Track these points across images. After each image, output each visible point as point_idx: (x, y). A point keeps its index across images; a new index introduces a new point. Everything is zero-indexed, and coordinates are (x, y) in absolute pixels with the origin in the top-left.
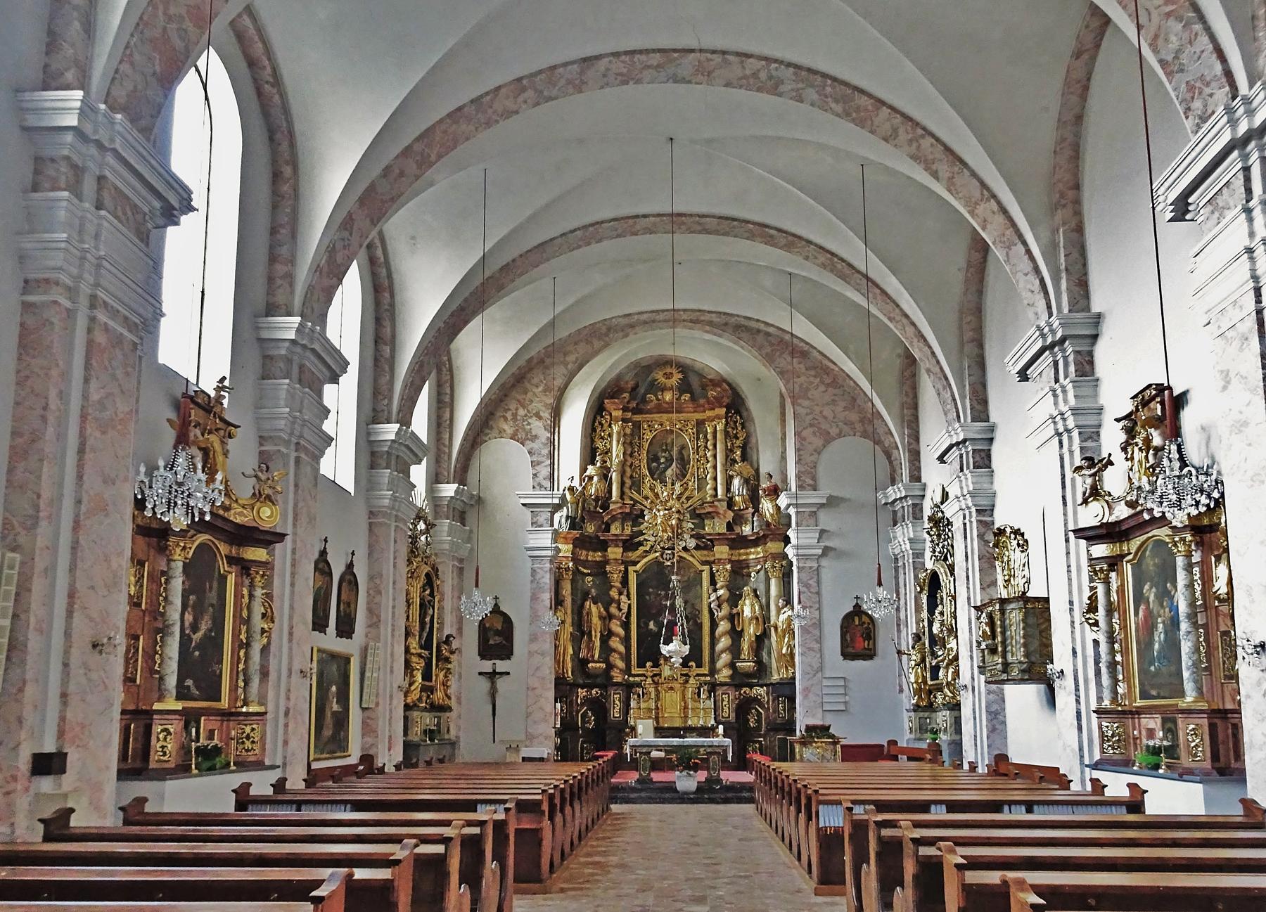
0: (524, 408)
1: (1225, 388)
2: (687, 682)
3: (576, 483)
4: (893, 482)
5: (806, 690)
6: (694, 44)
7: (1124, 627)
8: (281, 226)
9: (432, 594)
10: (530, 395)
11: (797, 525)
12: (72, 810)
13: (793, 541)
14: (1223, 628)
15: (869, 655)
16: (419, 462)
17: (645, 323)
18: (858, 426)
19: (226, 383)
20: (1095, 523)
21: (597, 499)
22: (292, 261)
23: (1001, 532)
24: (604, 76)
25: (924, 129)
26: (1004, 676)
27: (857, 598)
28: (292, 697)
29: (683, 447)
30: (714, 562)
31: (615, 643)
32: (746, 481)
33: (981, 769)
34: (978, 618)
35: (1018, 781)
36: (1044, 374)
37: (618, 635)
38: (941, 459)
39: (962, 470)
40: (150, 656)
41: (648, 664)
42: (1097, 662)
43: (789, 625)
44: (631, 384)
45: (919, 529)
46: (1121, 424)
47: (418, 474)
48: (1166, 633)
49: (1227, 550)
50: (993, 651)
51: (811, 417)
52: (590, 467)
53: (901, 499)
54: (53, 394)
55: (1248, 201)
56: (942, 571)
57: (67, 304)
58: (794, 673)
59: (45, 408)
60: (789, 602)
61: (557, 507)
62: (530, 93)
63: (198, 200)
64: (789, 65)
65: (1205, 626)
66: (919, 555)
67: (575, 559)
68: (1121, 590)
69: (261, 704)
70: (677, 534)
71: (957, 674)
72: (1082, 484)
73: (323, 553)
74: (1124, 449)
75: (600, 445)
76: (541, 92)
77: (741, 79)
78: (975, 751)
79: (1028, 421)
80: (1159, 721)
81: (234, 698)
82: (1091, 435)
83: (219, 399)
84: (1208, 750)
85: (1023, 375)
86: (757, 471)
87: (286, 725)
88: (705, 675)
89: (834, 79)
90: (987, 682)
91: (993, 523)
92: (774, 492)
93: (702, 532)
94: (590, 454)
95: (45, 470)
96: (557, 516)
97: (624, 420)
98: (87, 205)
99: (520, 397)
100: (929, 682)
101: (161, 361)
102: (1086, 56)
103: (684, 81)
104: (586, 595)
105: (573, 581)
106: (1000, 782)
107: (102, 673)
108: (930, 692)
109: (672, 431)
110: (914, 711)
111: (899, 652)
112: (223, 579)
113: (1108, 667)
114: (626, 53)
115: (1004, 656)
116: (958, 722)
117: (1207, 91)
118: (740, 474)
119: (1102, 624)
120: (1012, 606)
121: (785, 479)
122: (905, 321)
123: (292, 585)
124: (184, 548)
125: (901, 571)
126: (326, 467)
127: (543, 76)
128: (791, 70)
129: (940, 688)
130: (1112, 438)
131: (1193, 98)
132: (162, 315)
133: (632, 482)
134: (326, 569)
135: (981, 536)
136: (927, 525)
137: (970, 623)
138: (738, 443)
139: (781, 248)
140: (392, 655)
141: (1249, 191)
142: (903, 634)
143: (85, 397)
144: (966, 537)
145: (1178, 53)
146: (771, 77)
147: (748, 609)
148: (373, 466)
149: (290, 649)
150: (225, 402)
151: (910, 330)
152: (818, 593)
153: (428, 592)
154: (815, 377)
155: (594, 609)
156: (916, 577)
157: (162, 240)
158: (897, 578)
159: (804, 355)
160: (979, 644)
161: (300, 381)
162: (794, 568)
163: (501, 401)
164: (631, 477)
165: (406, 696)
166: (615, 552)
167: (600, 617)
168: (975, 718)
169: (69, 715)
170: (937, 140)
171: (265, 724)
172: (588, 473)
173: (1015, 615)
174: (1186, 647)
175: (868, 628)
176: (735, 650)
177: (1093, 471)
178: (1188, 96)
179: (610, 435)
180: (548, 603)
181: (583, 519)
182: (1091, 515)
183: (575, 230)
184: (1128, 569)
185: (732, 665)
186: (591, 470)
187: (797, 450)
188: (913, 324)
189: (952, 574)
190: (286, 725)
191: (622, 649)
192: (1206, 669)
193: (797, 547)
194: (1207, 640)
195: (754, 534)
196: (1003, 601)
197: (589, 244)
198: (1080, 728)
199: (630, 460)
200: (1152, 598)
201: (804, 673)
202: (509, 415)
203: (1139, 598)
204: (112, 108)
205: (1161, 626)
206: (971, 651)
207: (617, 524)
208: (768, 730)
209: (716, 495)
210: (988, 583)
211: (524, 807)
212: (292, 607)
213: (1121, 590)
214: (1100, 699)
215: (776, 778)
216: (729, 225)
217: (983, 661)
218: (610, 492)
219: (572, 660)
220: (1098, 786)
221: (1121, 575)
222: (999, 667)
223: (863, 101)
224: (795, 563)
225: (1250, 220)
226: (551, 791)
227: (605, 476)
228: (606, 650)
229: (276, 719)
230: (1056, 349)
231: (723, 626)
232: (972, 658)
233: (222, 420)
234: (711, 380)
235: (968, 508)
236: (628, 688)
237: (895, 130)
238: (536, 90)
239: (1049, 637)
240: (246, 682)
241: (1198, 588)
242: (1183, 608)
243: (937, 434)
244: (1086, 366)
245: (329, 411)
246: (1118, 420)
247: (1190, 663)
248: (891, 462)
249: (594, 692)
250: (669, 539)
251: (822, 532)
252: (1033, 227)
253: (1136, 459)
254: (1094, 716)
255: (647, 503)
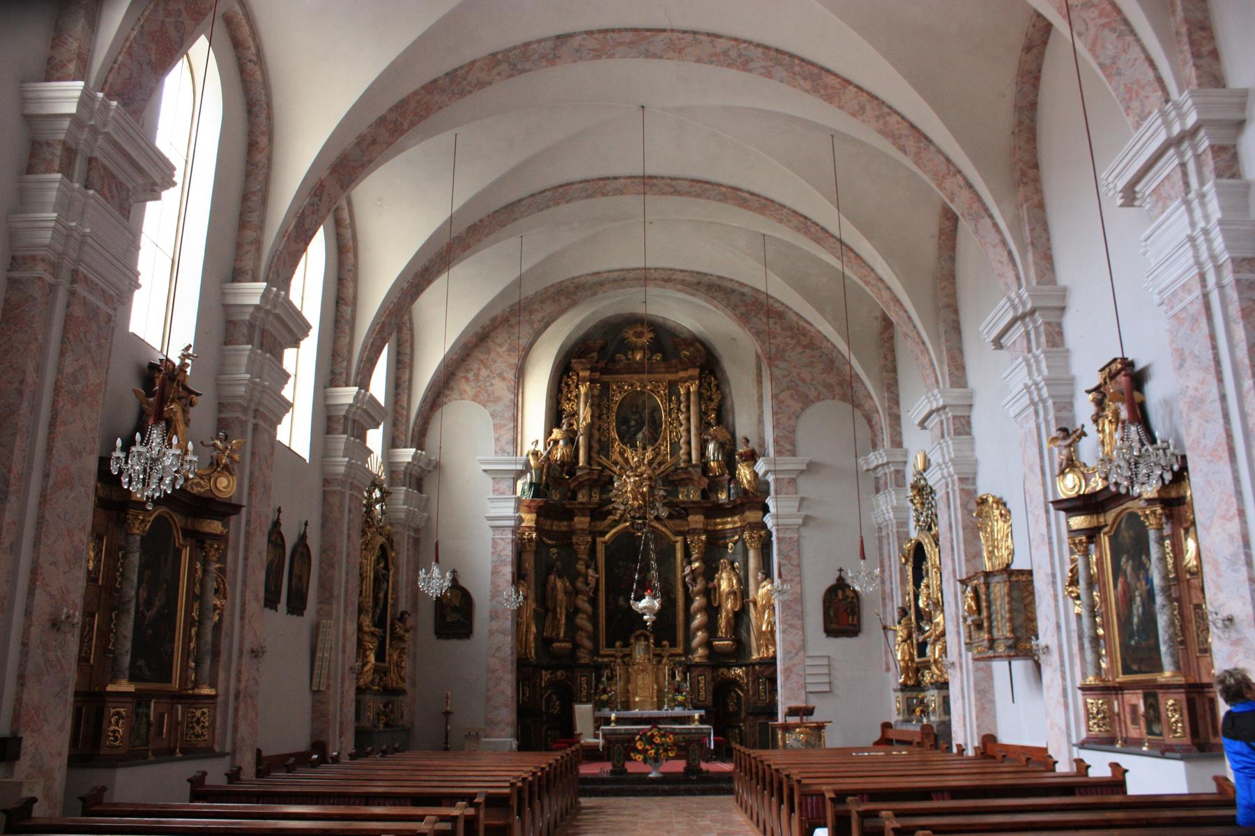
0: (486, 367)
1: (1181, 366)
2: (659, 662)
3: (540, 447)
4: (874, 447)
5: (787, 670)
6: (664, 24)
7: (1104, 599)
8: (254, 193)
9: (386, 568)
10: (493, 355)
11: (776, 492)
12: (34, 800)
13: (772, 510)
14: (1195, 601)
15: (853, 630)
16: (377, 427)
17: (615, 281)
18: (837, 390)
19: (191, 351)
20: (1072, 494)
21: (563, 464)
22: (261, 227)
23: (983, 502)
24: (577, 51)
25: (890, 107)
26: (991, 653)
27: (841, 570)
28: (244, 679)
29: (656, 409)
30: (688, 532)
31: (582, 620)
32: (721, 446)
33: (970, 752)
34: (964, 592)
35: (1006, 764)
36: (1018, 344)
37: (585, 612)
38: (922, 424)
39: (943, 436)
40: (105, 633)
41: (618, 644)
42: (1080, 638)
43: (769, 599)
44: (600, 343)
45: (903, 496)
46: (1090, 396)
47: (375, 439)
48: (1143, 605)
49: (1193, 523)
50: (979, 626)
51: (787, 379)
52: (555, 431)
53: (883, 465)
54: (30, 368)
55: (1187, 194)
56: (927, 542)
57: (49, 278)
58: (775, 652)
59: (22, 382)
60: (768, 575)
61: (520, 474)
62: (504, 66)
63: (178, 177)
64: (758, 45)
65: (1178, 600)
66: (903, 524)
67: (538, 528)
68: (1100, 563)
69: (213, 685)
70: (649, 501)
71: (944, 651)
72: (1059, 455)
73: (277, 524)
74: (1095, 421)
75: (567, 407)
76: (515, 65)
77: (711, 56)
78: (964, 735)
79: (1004, 390)
80: (1141, 696)
81: (184, 679)
82: (1065, 405)
83: (184, 365)
84: (1187, 725)
85: (998, 343)
86: (733, 435)
87: (236, 710)
88: (680, 655)
89: (802, 60)
90: (975, 660)
91: (975, 491)
92: (751, 457)
93: (675, 500)
94: (556, 416)
95: (18, 443)
96: (520, 483)
97: (592, 381)
98: (77, 185)
99: (482, 357)
100: (917, 660)
101: (132, 329)
102: (1035, 51)
103: (655, 56)
104: (550, 569)
105: (536, 553)
106: (989, 766)
107: (59, 653)
108: (918, 670)
109: (642, 393)
110: (902, 690)
111: (885, 628)
112: (178, 553)
113: (1091, 642)
114: (600, 31)
115: (990, 631)
116: (946, 702)
117: (1143, 93)
118: (714, 438)
119: (1083, 597)
120: (997, 579)
121: (762, 443)
122: (880, 285)
123: (246, 558)
124: (143, 521)
125: (885, 541)
126: (282, 434)
127: (517, 52)
128: (760, 50)
129: (927, 666)
130: (1084, 408)
131: (1131, 99)
132: (139, 286)
133: (598, 445)
134: (279, 542)
135: (964, 506)
136: (910, 494)
137: (956, 596)
138: (712, 405)
139: (755, 211)
140: (344, 634)
141: (1187, 184)
142: (889, 609)
143: (60, 370)
144: (949, 507)
145: (1114, 60)
146: (740, 55)
147: (725, 583)
148: (329, 431)
149: (242, 627)
150: (188, 370)
151: (886, 294)
152: (799, 566)
153: (382, 565)
154: (792, 338)
155: (559, 584)
156: (901, 548)
157: (1006, 747)
158: (881, 548)
159: (780, 315)
160: (965, 619)
161: (261, 346)
162: (774, 539)
163: (463, 360)
164: (599, 441)
165: (358, 679)
166: (581, 522)
167: (566, 592)
168: (963, 697)
169: (25, 697)
170: (903, 118)
171: (215, 708)
172: (553, 436)
173: (999, 589)
174: (1162, 620)
175: (852, 603)
176: (711, 627)
177: (1068, 441)
178: (1127, 96)
179: (577, 397)
180: (509, 577)
181: (547, 486)
182: (1069, 486)
183: (544, 191)
184: (1105, 541)
185: (708, 644)
186: (556, 433)
187: (774, 413)
188: (889, 288)
189: (937, 545)
190: (236, 710)
191: (589, 626)
192: (1182, 643)
193: (777, 516)
194: (1181, 613)
195: (730, 502)
196: (987, 575)
197: (557, 204)
198: (1066, 706)
199: (597, 423)
200: (1129, 570)
201: (786, 652)
202: (471, 375)
203: (1117, 571)
204: (109, 96)
205: (1138, 599)
206: (958, 625)
207: (585, 491)
208: (749, 714)
209: (690, 460)
210: (973, 555)
211: (494, 801)
212: (244, 583)
213: (1100, 563)
214: (1084, 675)
215: (757, 767)
216: (701, 188)
217: (970, 637)
218: (577, 456)
219: (536, 639)
220: (1082, 767)
221: (1099, 546)
222: (986, 643)
223: (830, 80)
224: (774, 531)
225: (1190, 211)
226: (520, 784)
227: (571, 439)
228: (572, 627)
229: (226, 702)
230: (1027, 320)
231: (698, 601)
232: (959, 633)
233: (186, 388)
234: (684, 340)
235: (950, 476)
236: (598, 668)
237: (862, 108)
238: (510, 64)
239: (1033, 612)
240: (198, 662)
241: (1170, 561)
242: (1157, 581)
243: (916, 405)
244: (1055, 336)
245: (288, 376)
246: (1089, 392)
247: (1167, 637)
248: (871, 427)
249: (559, 674)
250: (640, 507)
251: (802, 500)
252: (998, 204)
253: (1107, 431)
254: (1079, 692)
255: (616, 469)
